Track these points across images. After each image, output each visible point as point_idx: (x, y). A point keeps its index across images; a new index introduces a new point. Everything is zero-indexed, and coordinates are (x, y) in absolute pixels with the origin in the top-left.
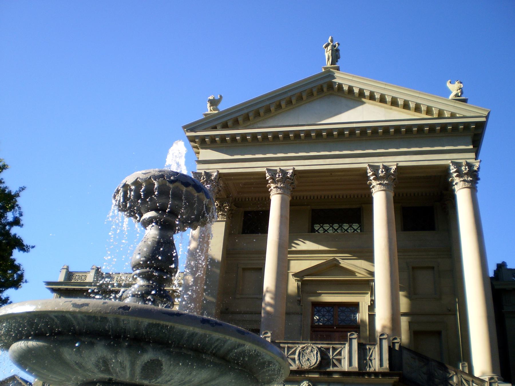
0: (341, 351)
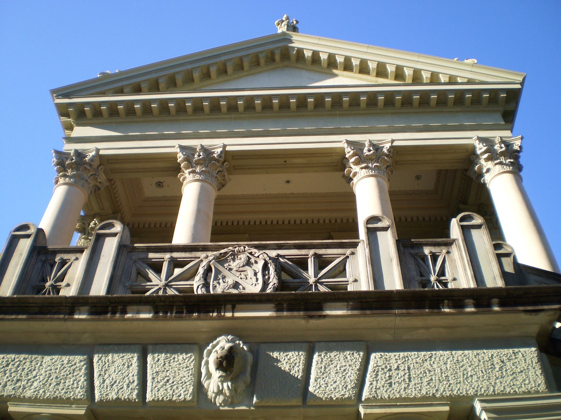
0: (343, 264)
